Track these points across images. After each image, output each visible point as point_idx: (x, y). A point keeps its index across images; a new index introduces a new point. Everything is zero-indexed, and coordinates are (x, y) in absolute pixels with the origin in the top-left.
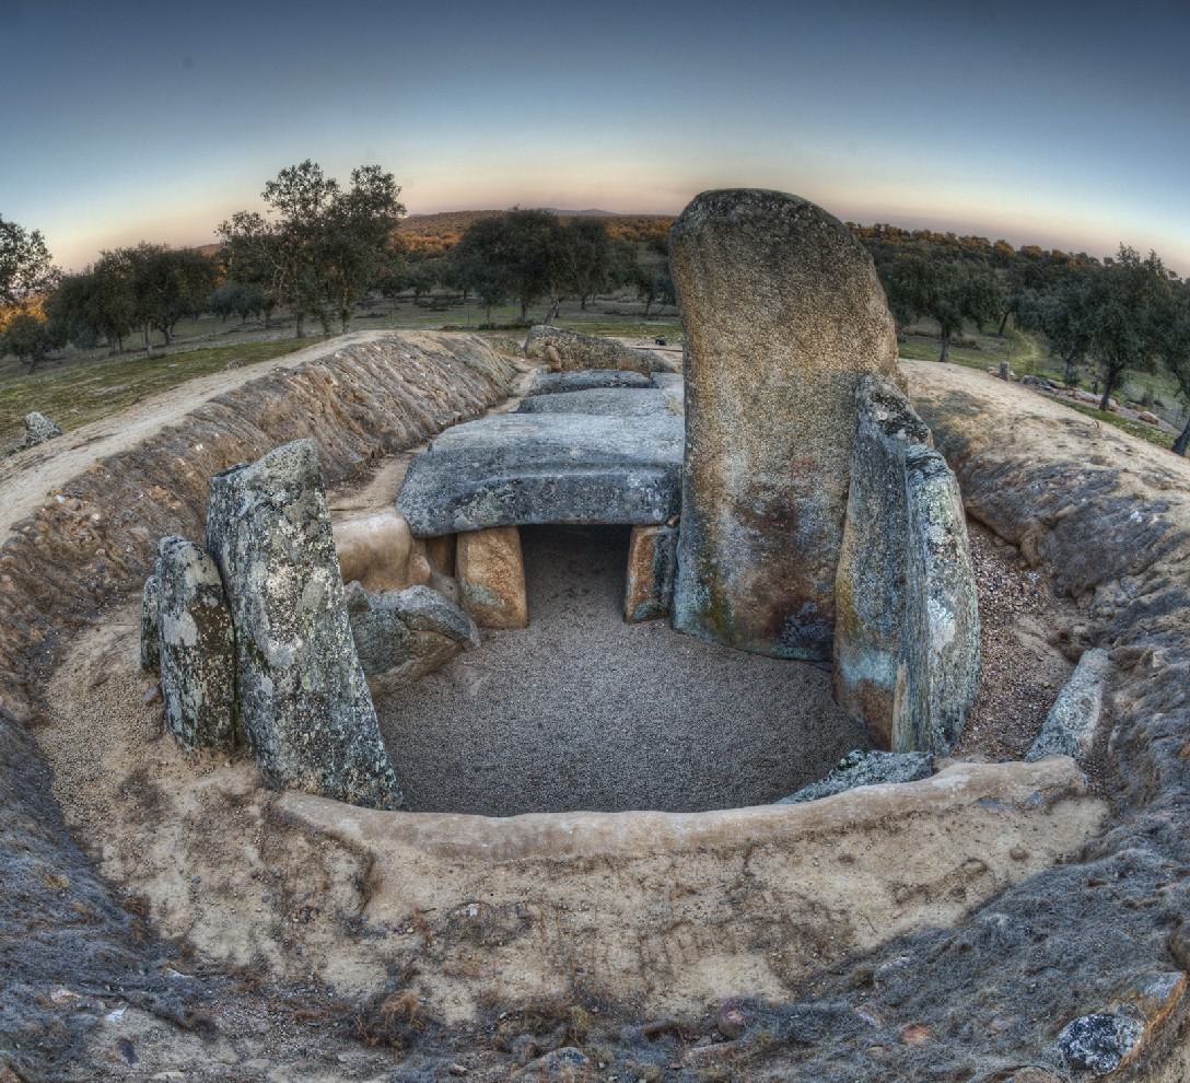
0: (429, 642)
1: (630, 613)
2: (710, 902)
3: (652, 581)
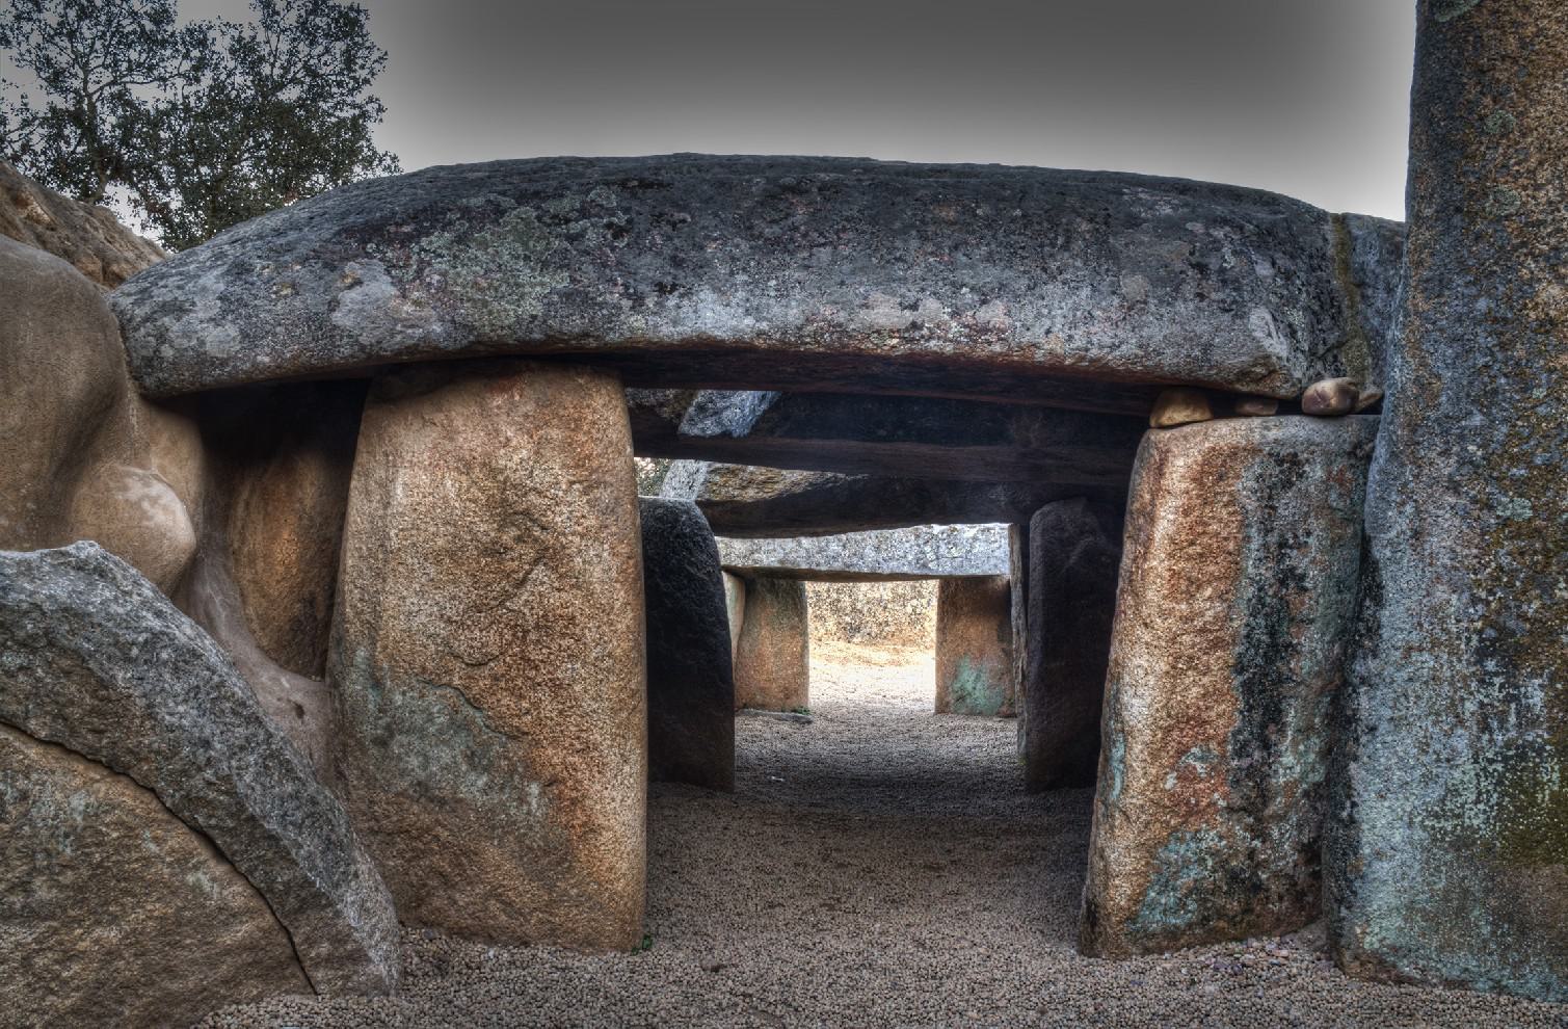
0: (86, 836)
1: (1120, 893)
2: (1420, 432)
3: (1225, 716)
